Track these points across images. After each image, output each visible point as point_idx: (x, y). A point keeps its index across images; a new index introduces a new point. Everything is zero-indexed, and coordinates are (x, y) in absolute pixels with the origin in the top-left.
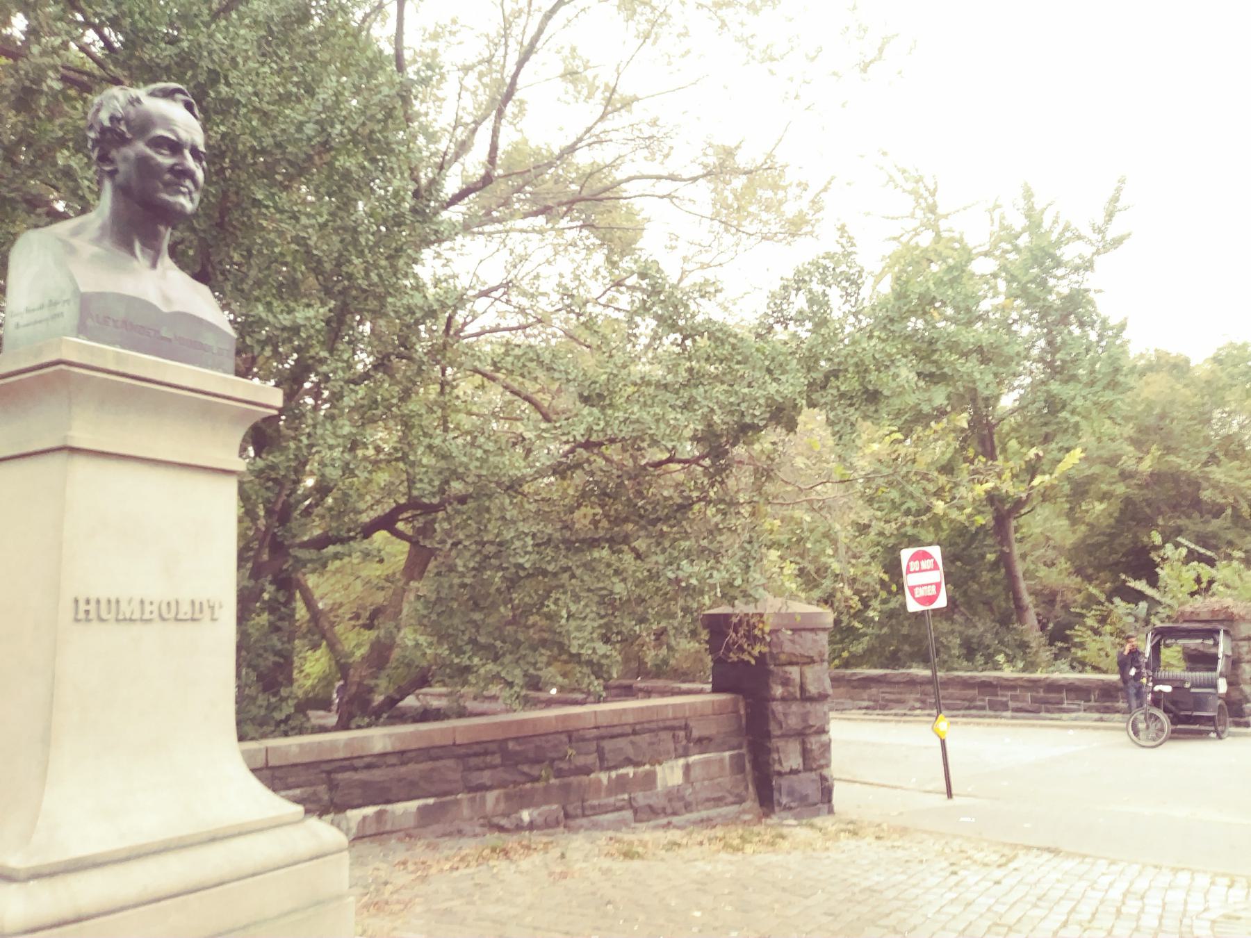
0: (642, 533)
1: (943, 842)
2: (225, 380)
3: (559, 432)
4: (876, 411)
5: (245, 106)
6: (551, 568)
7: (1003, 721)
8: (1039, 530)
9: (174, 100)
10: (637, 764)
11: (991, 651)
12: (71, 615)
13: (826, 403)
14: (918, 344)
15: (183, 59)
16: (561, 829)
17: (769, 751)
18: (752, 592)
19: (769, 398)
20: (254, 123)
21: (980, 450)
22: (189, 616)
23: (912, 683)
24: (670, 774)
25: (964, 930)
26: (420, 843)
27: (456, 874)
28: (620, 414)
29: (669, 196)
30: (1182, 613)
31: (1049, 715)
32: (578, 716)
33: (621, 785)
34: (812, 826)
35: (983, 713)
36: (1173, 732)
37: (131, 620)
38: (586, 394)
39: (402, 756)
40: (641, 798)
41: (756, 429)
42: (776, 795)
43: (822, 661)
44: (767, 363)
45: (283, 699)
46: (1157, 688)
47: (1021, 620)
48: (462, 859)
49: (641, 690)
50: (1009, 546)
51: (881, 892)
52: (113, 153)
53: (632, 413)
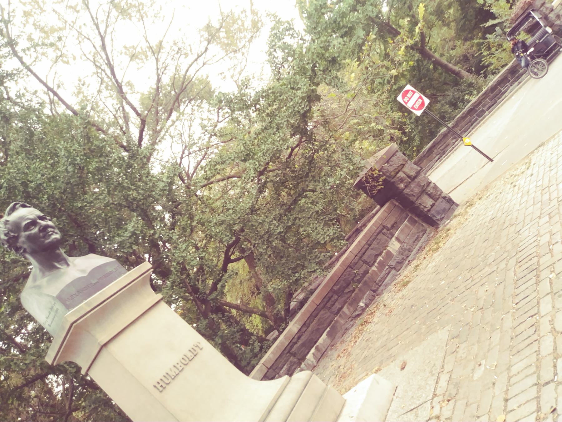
0: (307, 183)
1: (502, 179)
2: (127, 276)
3: (246, 180)
4: (340, 64)
5: (44, 183)
6: (290, 224)
7: (487, 117)
8: (439, 40)
9: (17, 209)
10: (380, 254)
11: (461, 98)
12: (158, 392)
13: (321, 79)
14: (331, 27)
15: (9, 189)
16: (377, 297)
17: (418, 207)
18: (360, 166)
19: (303, 98)
20: (53, 185)
21: (391, 36)
22: (193, 356)
23: (445, 135)
24: (394, 246)
25: (534, 203)
26: (338, 345)
27: (357, 344)
28: (260, 154)
29: (204, 64)
30: (512, 19)
31: (501, 99)
32: (347, 258)
33: (382, 265)
34: (455, 216)
35: (478, 121)
36: (548, 61)
37: (177, 375)
38: (243, 158)
39: (305, 325)
40: (392, 263)
41: (309, 111)
42: (434, 218)
43: (407, 161)
44: (289, 86)
45: (253, 344)
46: (528, 53)
47: (462, 78)
48: (355, 338)
49: (361, 227)
50: (433, 57)
51: (496, 217)
52: (18, 245)
53: (263, 149)
